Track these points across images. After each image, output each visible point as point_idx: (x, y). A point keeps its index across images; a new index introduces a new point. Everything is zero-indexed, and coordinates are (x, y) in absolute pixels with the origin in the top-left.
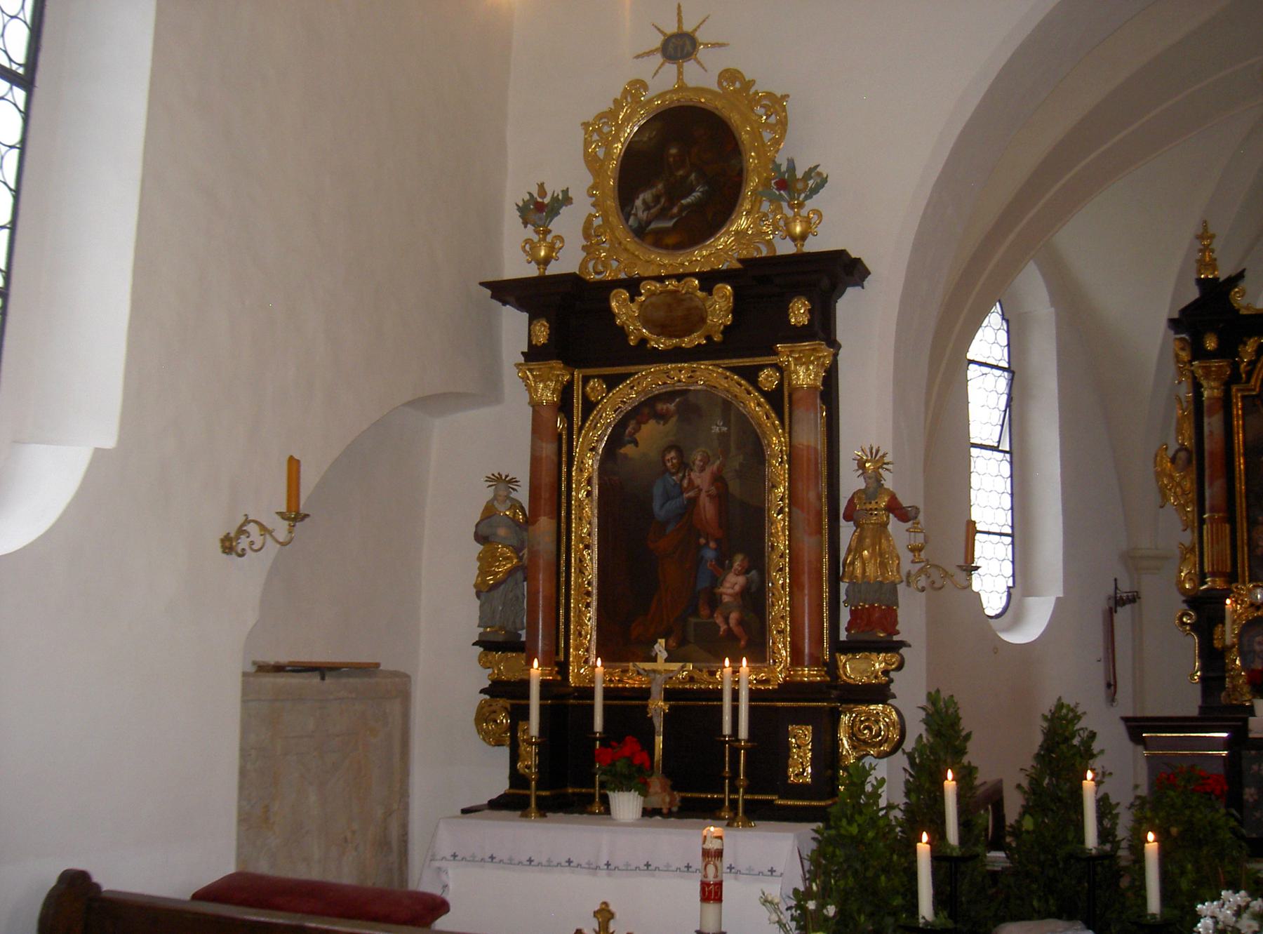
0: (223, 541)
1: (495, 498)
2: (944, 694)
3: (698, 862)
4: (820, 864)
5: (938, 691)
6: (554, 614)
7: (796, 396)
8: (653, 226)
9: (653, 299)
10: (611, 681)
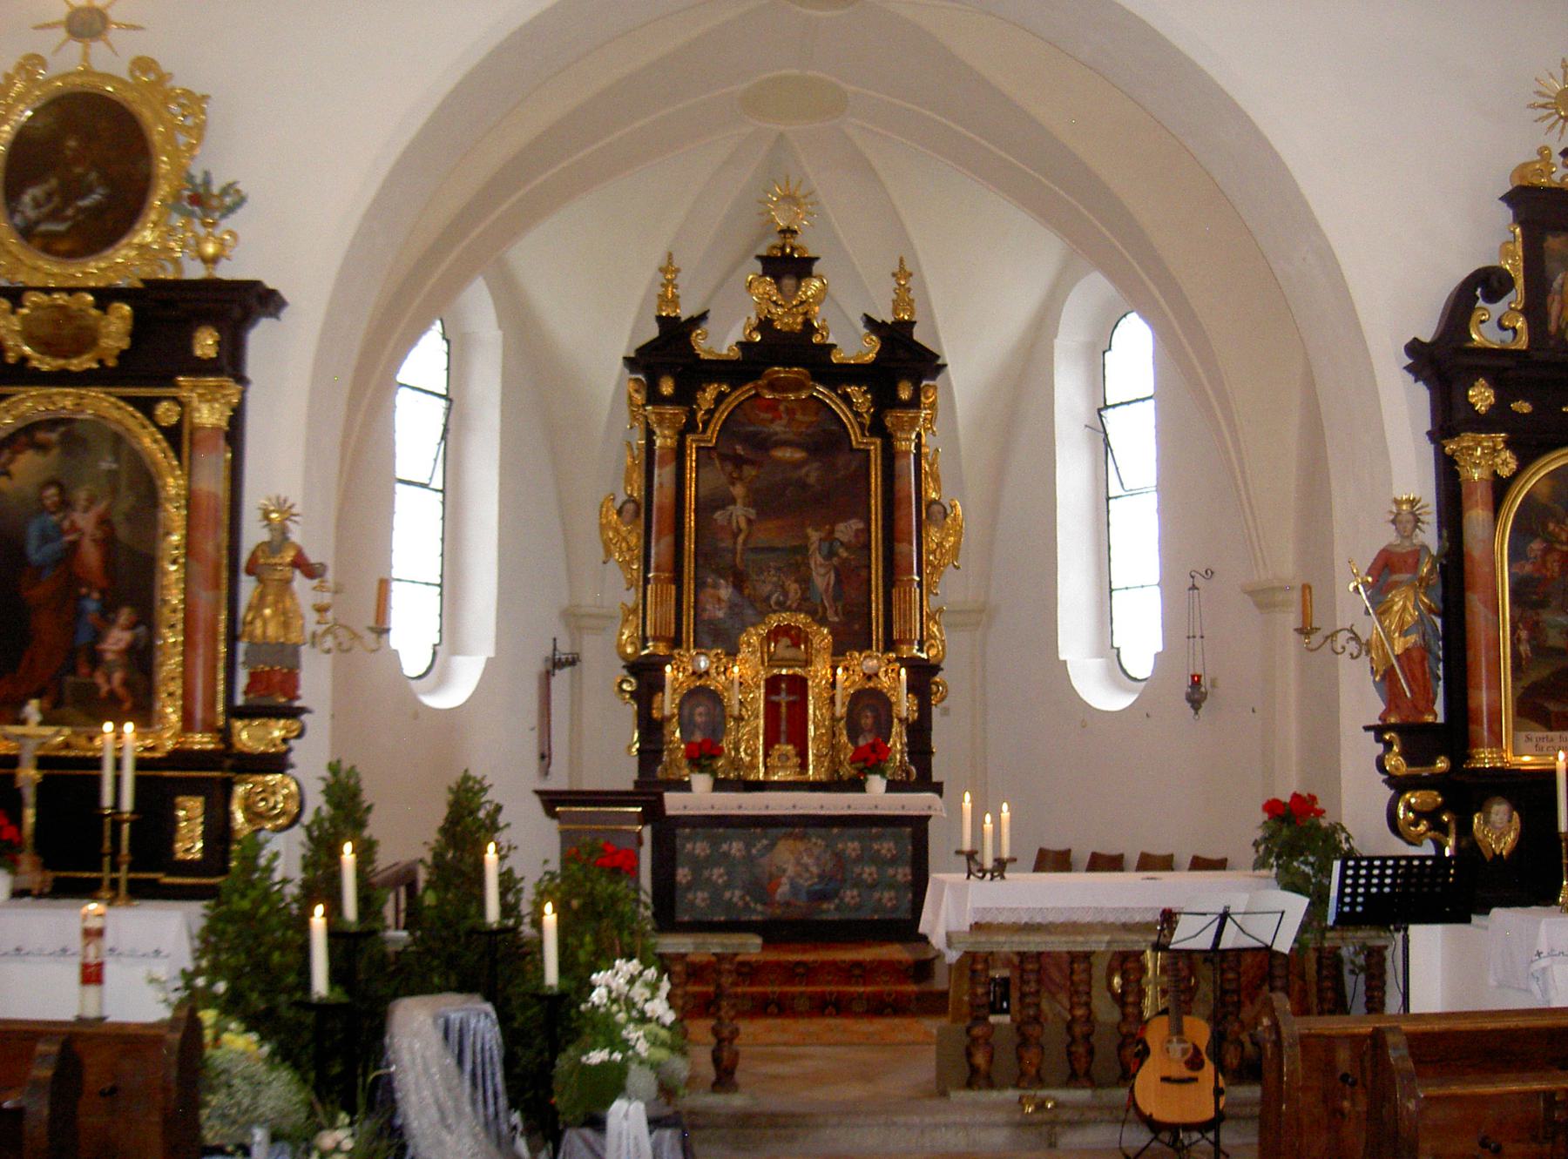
2: (346, 765)
3: (76, 942)
4: (210, 941)
7: (198, 435)
9: (40, 313)
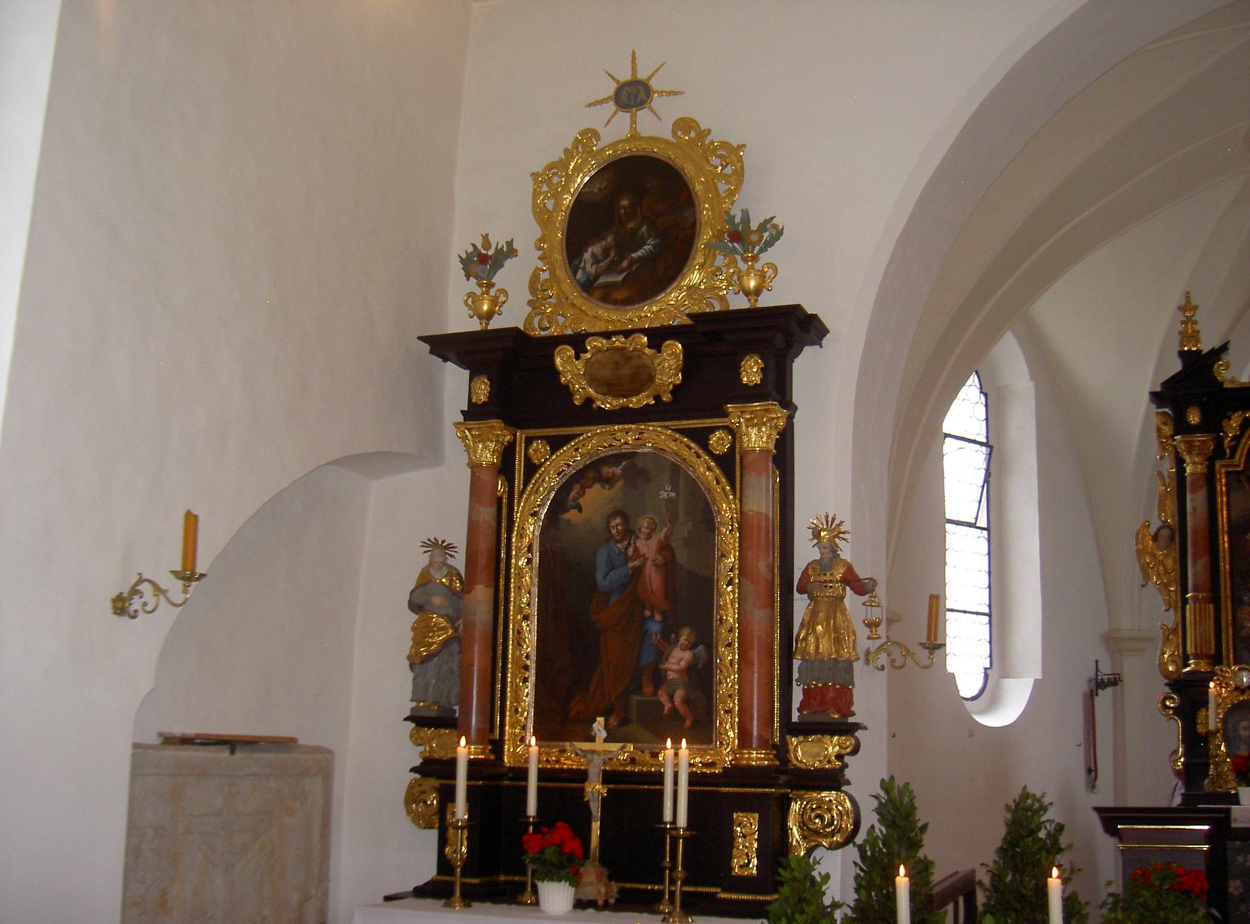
0: (114, 601)
1: (430, 564)
2: (899, 782)
5: (892, 778)
6: (488, 688)
7: (749, 459)
8: (601, 280)
10: (547, 761)
